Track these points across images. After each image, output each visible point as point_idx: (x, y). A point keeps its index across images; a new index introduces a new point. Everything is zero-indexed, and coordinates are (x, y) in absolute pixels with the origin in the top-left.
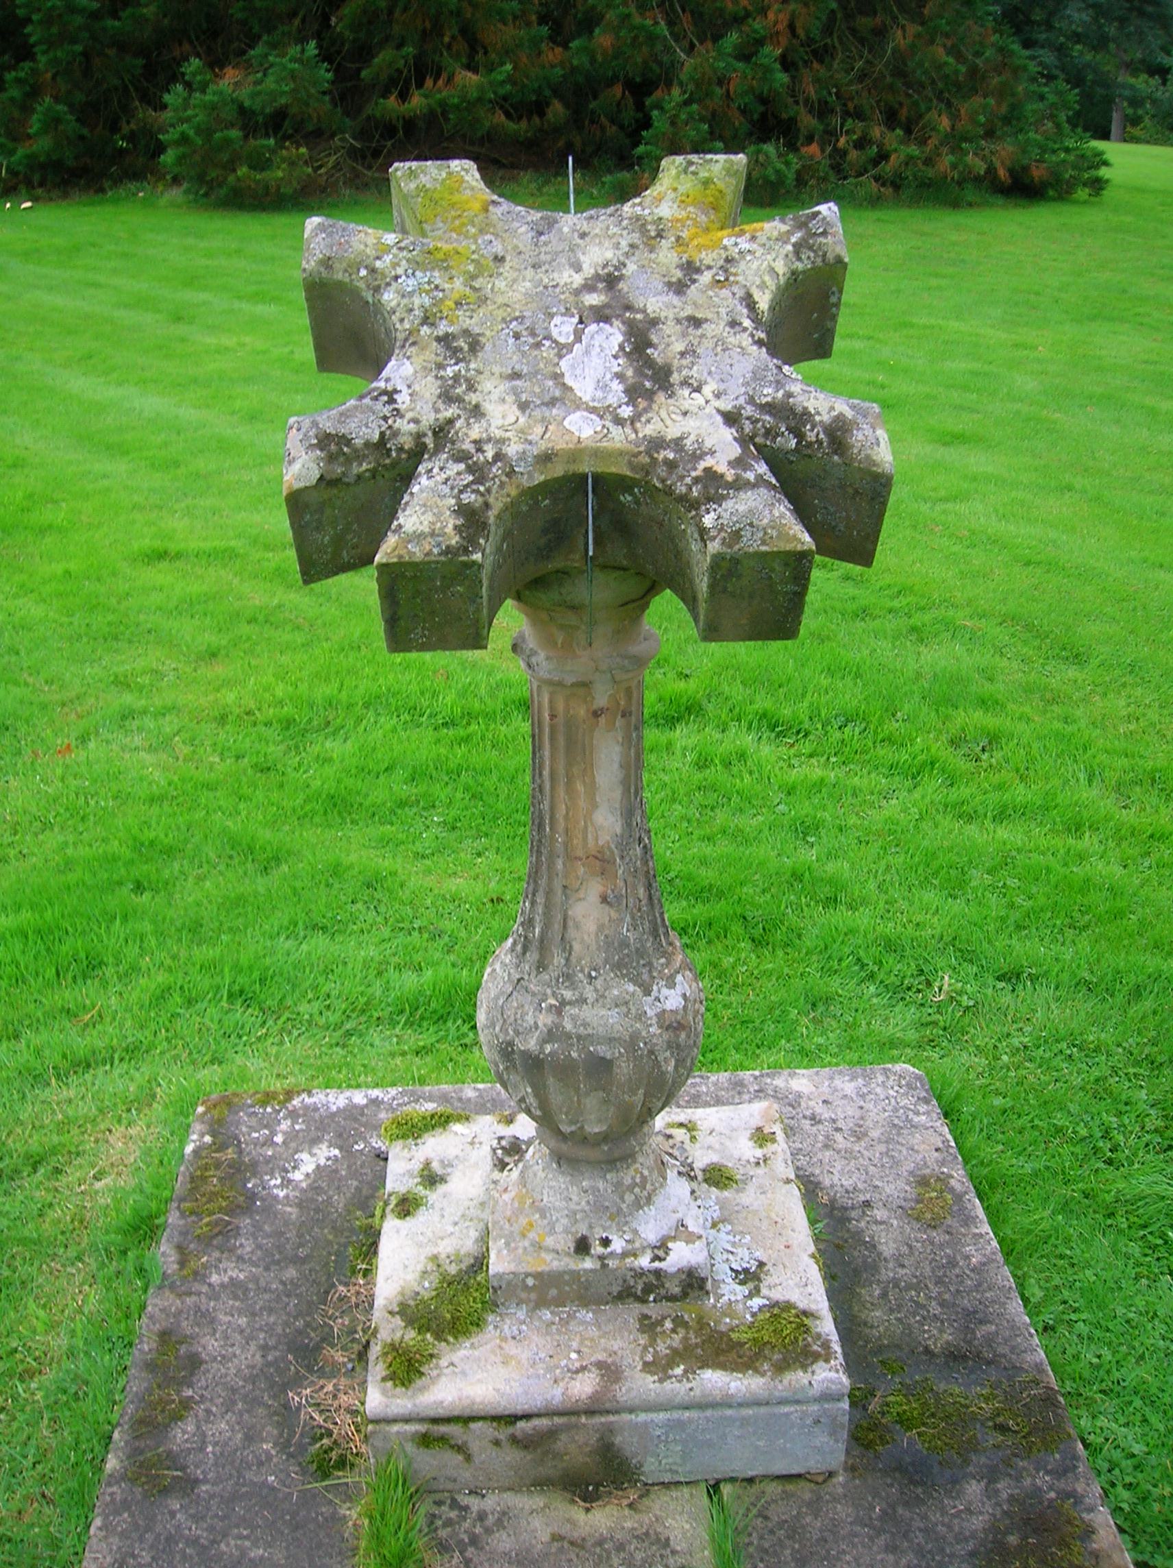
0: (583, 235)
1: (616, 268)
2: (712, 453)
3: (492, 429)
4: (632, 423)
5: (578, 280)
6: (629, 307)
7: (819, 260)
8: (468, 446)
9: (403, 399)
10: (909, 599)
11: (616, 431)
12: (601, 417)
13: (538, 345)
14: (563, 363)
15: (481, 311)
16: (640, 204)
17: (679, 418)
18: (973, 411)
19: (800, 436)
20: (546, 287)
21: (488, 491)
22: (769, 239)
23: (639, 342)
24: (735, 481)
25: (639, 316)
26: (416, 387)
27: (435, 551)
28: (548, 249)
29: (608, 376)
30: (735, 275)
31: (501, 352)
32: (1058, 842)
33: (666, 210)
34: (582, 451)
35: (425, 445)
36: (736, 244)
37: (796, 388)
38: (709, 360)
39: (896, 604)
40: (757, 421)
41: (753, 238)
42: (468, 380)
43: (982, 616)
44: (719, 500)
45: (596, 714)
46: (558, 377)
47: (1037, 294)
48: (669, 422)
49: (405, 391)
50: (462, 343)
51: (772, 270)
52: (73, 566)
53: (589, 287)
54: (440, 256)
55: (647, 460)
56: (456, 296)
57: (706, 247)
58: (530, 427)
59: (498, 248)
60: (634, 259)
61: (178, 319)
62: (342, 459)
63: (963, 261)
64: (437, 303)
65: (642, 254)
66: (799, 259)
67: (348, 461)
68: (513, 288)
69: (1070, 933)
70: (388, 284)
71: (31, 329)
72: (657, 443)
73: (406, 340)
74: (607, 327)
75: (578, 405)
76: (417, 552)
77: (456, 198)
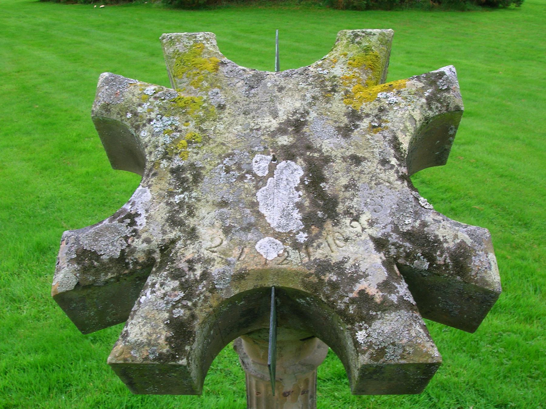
0: (281, 89)
1: (303, 116)
2: (365, 276)
3: (203, 250)
4: (307, 248)
5: (274, 124)
6: (309, 148)
7: (444, 109)
8: (183, 265)
9: (141, 221)
10: (450, 194)
11: (294, 255)
12: (283, 242)
13: (242, 178)
14: (260, 194)
15: (205, 148)
16: (321, 66)
17: (341, 244)
18: (475, 101)
19: (431, 259)
20: (251, 130)
21: (195, 305)
22: (410, 93)
23: (315, 178)
24: (383, 302)
25: (316, 155)
26: (152, 212)
27: (151, 357)
28: (256, 99)
29: (291, 206)
30: (386, 122)
31: (216, 183)
32: (521, 326)
33: (338, 71)
34: (267, 271)
35: (154, 260)
36: (387, 97)
37: (429, 218)
38: (366, 193)
39: (444, 196)
40: (400, 246)
41: (399, 92)
42: (189, 207)
43: (483, 203)
44: (369, 320)
45: (285, 395)
46: (254, 205)
47: (497, 48)
48: (334, 247)
49: (144, 214)
50: (188, 175)
51: (412, 118)
52: (90, 170)
53: (282, 130)
54: (181, 104)
55: (316, 280)
56: (188, 136)
57: (365, 99)
58: (230, 250)
59: (222, 98)
60: (315, 108)
61: (152, 55)
62: (93, 270)
63: (467, 34)
64: (175, 141)
65: (321, 104)
66: (430, 109)
67: (97, 271)
68: (228, 130)
69: (530, 381)
70: (144, 125)
71: (94, 58)
72: (324, 266)
73: (151, 170)
74: (293, 163)
75: (268, 231)
76: (138, 357)
77: (198, 60)
